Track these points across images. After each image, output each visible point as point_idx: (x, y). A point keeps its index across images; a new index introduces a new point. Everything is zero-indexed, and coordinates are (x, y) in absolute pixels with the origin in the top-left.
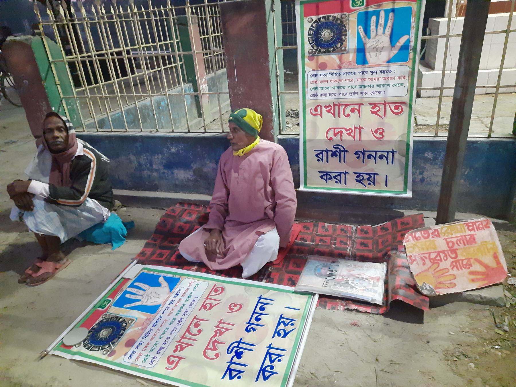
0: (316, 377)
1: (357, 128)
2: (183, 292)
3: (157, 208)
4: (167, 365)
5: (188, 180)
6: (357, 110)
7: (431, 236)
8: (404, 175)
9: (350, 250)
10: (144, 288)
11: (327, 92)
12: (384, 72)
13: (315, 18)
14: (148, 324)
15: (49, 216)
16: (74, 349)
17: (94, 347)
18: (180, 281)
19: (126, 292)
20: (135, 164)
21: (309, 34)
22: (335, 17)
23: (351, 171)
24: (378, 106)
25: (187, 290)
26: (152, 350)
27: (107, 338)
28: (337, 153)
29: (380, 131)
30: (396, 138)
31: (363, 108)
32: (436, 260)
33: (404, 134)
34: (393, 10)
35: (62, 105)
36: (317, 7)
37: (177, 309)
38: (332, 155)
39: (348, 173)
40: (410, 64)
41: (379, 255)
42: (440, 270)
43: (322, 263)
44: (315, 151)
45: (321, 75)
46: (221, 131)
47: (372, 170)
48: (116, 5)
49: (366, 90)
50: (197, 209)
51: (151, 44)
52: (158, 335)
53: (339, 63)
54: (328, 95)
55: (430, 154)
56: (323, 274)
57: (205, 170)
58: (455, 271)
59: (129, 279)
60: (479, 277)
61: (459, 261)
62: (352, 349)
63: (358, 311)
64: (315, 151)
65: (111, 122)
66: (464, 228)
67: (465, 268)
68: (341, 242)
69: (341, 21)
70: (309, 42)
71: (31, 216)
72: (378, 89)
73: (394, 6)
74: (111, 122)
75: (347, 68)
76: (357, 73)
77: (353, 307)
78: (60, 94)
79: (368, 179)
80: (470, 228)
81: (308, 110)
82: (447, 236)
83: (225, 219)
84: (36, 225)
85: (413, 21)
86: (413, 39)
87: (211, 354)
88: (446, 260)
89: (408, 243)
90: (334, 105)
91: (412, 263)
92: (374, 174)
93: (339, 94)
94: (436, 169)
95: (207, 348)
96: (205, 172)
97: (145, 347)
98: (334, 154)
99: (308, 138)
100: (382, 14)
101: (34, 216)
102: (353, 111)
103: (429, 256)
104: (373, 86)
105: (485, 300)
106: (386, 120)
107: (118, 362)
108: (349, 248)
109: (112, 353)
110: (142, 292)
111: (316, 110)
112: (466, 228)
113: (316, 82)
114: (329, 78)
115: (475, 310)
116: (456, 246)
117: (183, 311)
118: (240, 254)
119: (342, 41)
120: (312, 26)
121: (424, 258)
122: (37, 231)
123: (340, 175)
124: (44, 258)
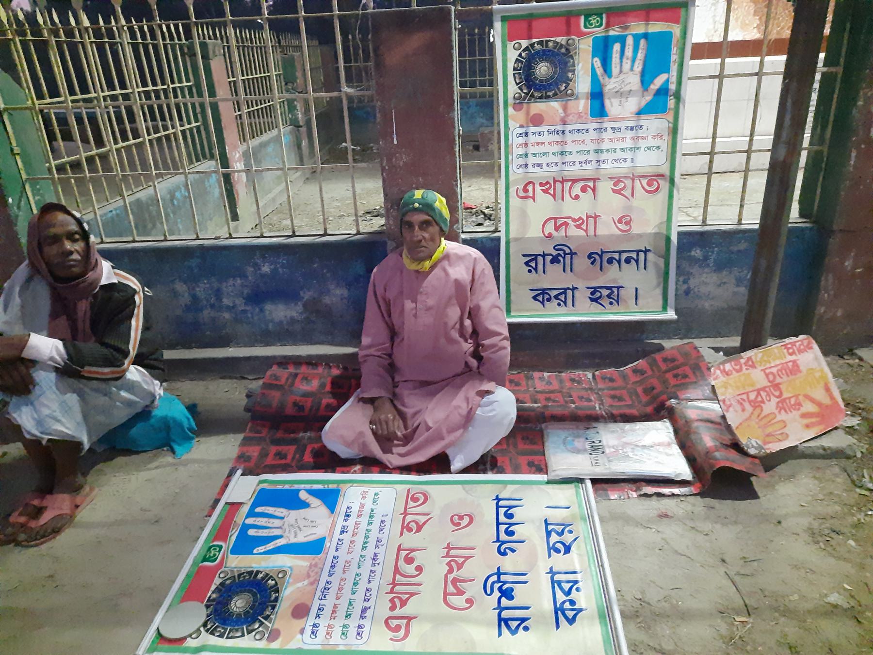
0: (649, 604)
1: (591, 217)
2: (355, 509)
3: (231, 378)
4: (391, 634)
5: (292, 321)
6: (590, 187)
7: (744, 368)
8: (662, 285)
9: (600, 409)
10: (277, 514)
11: (543, 160)
12: (632, 129)
13: (525, 43)
14: (317, 573)
15: (64, 402)
16: (191, 643)
17: (231, 631)
18: (342, 493)
19: (245, 527)
20: (186, 299)
21: (515, 69)
22: (558, 43)
23: (581, 285)
24: (622, 181)
25: (362, 506)
26: (348, 616)
27: (248, 612)
28: (560, 258)
29: (625, 220)
30: (651, 229)
31: (599, 185)
32: (757, 402)
33: (661, 223)
34: (646, 36)
35: (24, 194)
36: (530, 27)
37: (360, 540)
38: (552, 262)
39: (577, 288)
40: (671, 118)
41: (649, 410)
42: (765, 417)
43: (571, 432)
44: (524, 255)
45: (534, 133)
46: (354, 232)
47: (615, 280)
48: (155, 7)
49: (604, 156)
50: (315, 371)
51: (119, 91)
52: (348, 587)
53: (563, 115)
54: (544, 166)
55: (698, 251)
56: (581, 448)
57: (327, 300)
58: (783, 416)
59: (241, 504)
60: (814, 420)
61: (785, 399)
62: (680, 551)
63: (660, 495)
64: (524, 255)
65: (101, 226)
66: (783, 352)
67: (794, 409)
68: (581, 398)
69: (567, 49)
70: (515, 81)
71: (27, 405)
72: (623, 155)
73: (647, 29)
74: (101, 226)
75: (574, 122)
76: (591, 131)
77: (649, 490)
78: (21, 172)
79: (609, 296)
80: (791, 351)
81: (512, 190)
82: (764, 365)
83: (393, 379)
84: (39, 423)
85: (675, 52)
86: (674, 79)
87: (455, 600)
88: (770, 400)
89: (716, 381)
90: (555, 181)
91: (727, 411)
92: (619, 288)
93: (563, 163)
94: (707, 273)
95: (446, 594)
96: (326, 305)
97: (333, 613)
98: (555, 260)
99: (512, 236)
100: (630, 41)
101: (32, 404)
102: (584, 189)
103: (748, 398)
104: (615, 150)
105: (829, 452)
106: (635, 202)
107: (294, 647)
108: (597, 406)
109: (274, 635)
110: (277, 523)
111: (525, 190)
112: (785, 351)
113: (526, 145)
114: (547, 138)
115: (818, 468)
116: (778, 380)
117: (372, 541)
118: (444, 431)
119: (567, 81)
120: (520, 55)
121: (741, 401)
122: (41, 433)
123: (565, 293)
124: (47, 489)
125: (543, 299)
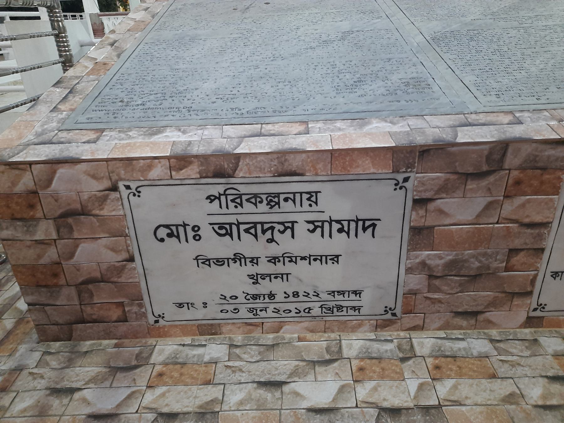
125: (256, 201)
